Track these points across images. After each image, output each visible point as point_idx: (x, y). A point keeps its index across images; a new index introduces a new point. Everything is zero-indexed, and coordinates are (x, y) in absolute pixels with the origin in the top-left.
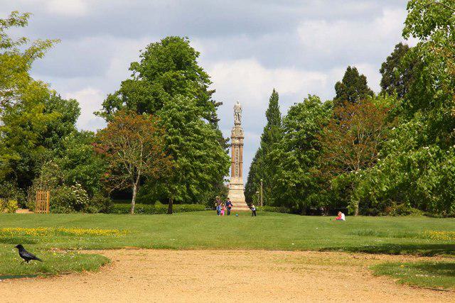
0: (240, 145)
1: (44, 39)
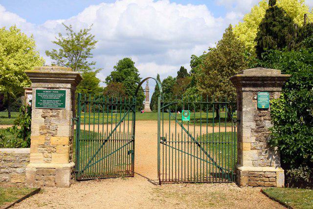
0: (148, 92)
1: (100, 68)
